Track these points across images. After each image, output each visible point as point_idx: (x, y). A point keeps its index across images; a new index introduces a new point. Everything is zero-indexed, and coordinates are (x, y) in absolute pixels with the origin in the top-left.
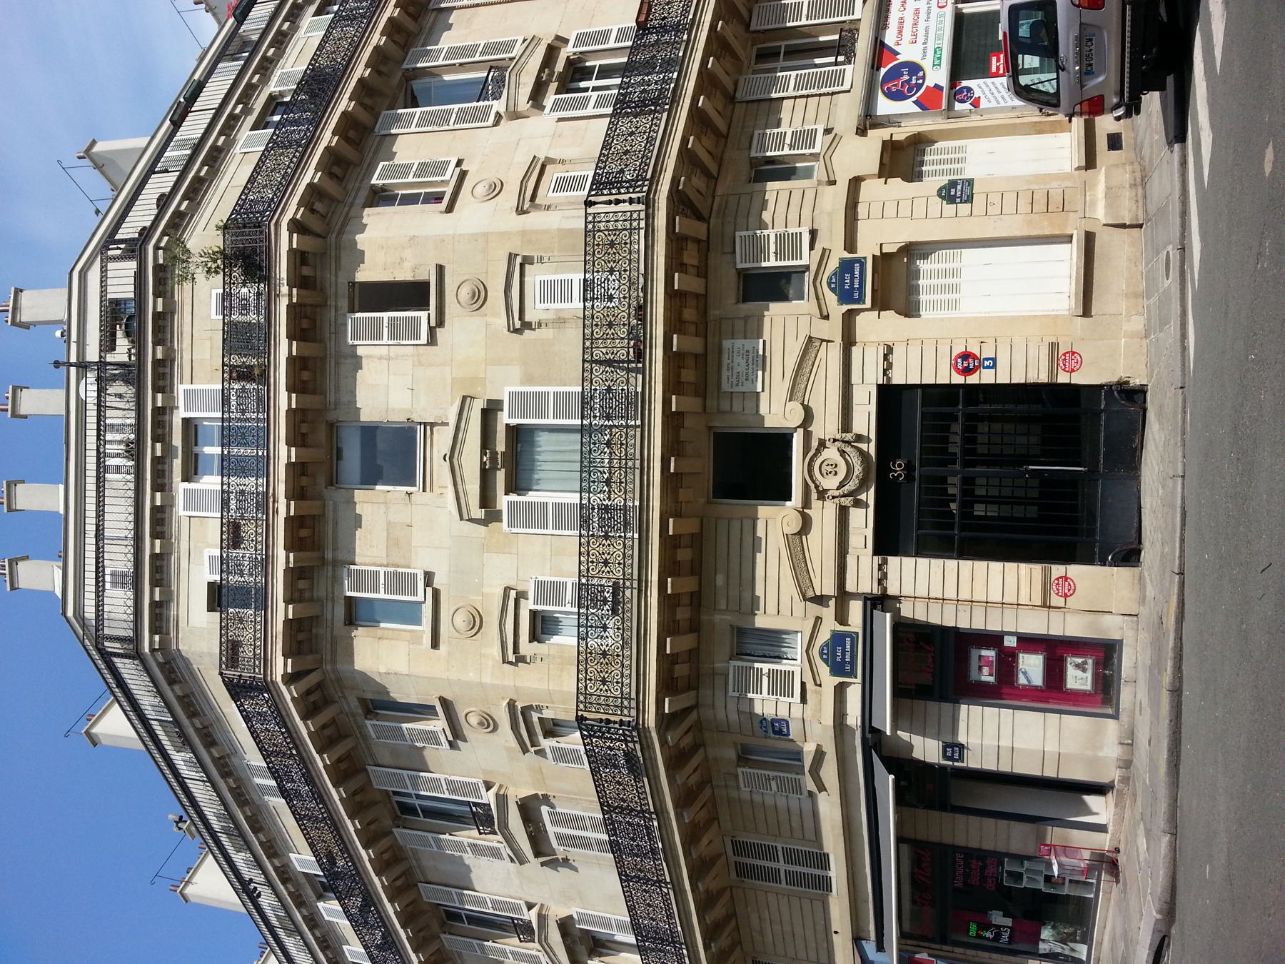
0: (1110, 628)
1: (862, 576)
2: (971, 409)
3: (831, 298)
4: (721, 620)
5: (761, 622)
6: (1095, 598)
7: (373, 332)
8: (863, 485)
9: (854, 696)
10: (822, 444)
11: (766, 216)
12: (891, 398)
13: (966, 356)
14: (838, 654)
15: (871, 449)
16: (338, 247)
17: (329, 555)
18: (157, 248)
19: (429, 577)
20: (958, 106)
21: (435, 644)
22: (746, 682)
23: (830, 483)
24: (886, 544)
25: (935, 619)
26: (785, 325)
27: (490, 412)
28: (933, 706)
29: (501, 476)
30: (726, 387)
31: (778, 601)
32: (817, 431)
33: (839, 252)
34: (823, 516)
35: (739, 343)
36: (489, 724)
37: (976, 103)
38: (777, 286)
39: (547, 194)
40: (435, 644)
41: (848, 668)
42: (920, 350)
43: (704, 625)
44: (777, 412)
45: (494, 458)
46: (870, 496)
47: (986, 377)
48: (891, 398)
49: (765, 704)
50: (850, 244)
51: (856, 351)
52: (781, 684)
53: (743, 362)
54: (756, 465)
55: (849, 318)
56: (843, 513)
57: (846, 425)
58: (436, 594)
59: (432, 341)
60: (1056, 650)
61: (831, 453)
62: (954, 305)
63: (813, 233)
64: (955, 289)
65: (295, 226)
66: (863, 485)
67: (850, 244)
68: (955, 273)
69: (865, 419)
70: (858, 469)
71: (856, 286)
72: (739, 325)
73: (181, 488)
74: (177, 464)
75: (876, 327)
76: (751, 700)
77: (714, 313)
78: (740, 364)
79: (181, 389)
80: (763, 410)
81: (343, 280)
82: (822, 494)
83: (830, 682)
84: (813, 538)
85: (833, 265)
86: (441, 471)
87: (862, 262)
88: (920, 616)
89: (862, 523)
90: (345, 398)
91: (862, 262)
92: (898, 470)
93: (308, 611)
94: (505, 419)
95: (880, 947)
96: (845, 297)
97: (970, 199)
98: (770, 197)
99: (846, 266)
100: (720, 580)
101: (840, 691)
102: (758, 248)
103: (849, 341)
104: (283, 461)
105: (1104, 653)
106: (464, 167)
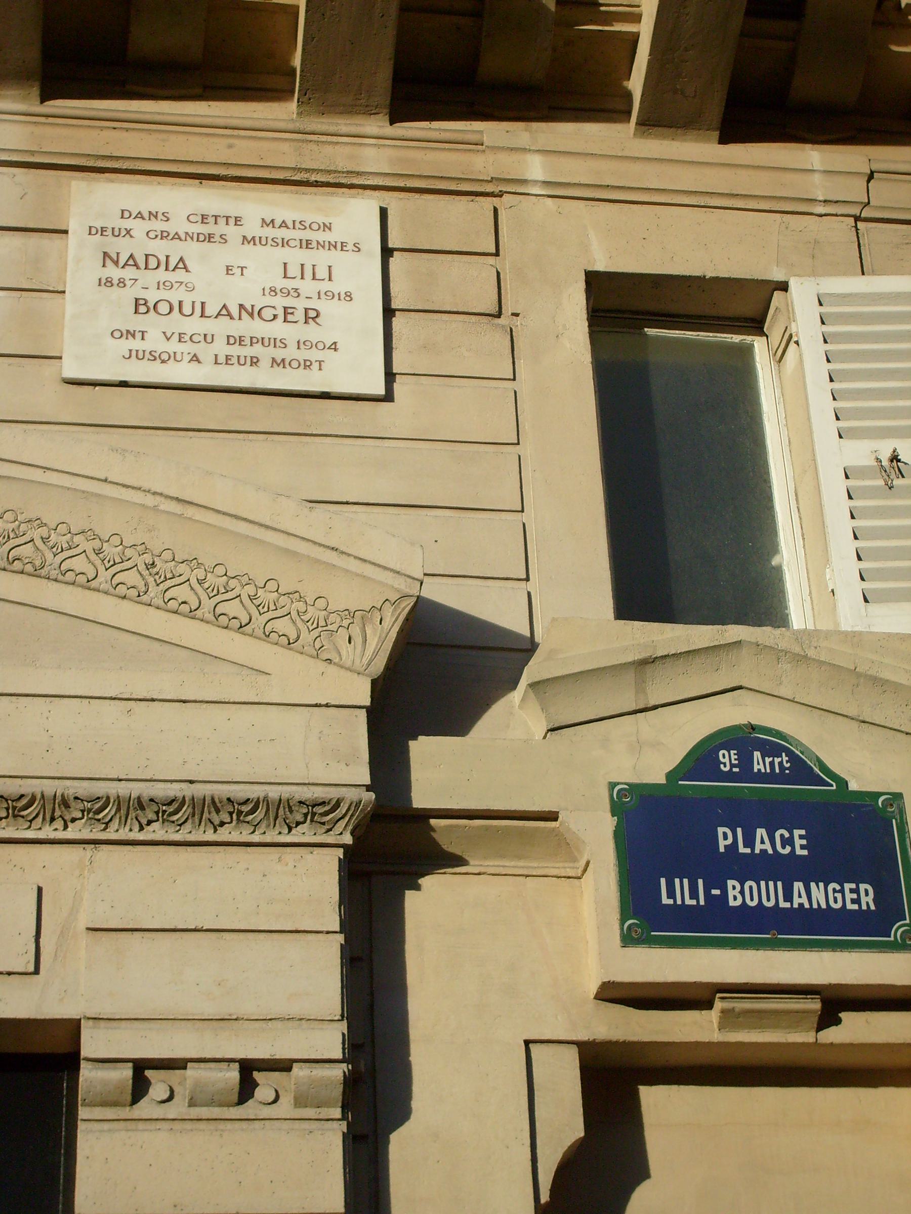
3: (654, 751)
30: (92, 203)
41: (680, 893)
53: (244, 289)
71: (737, 894)
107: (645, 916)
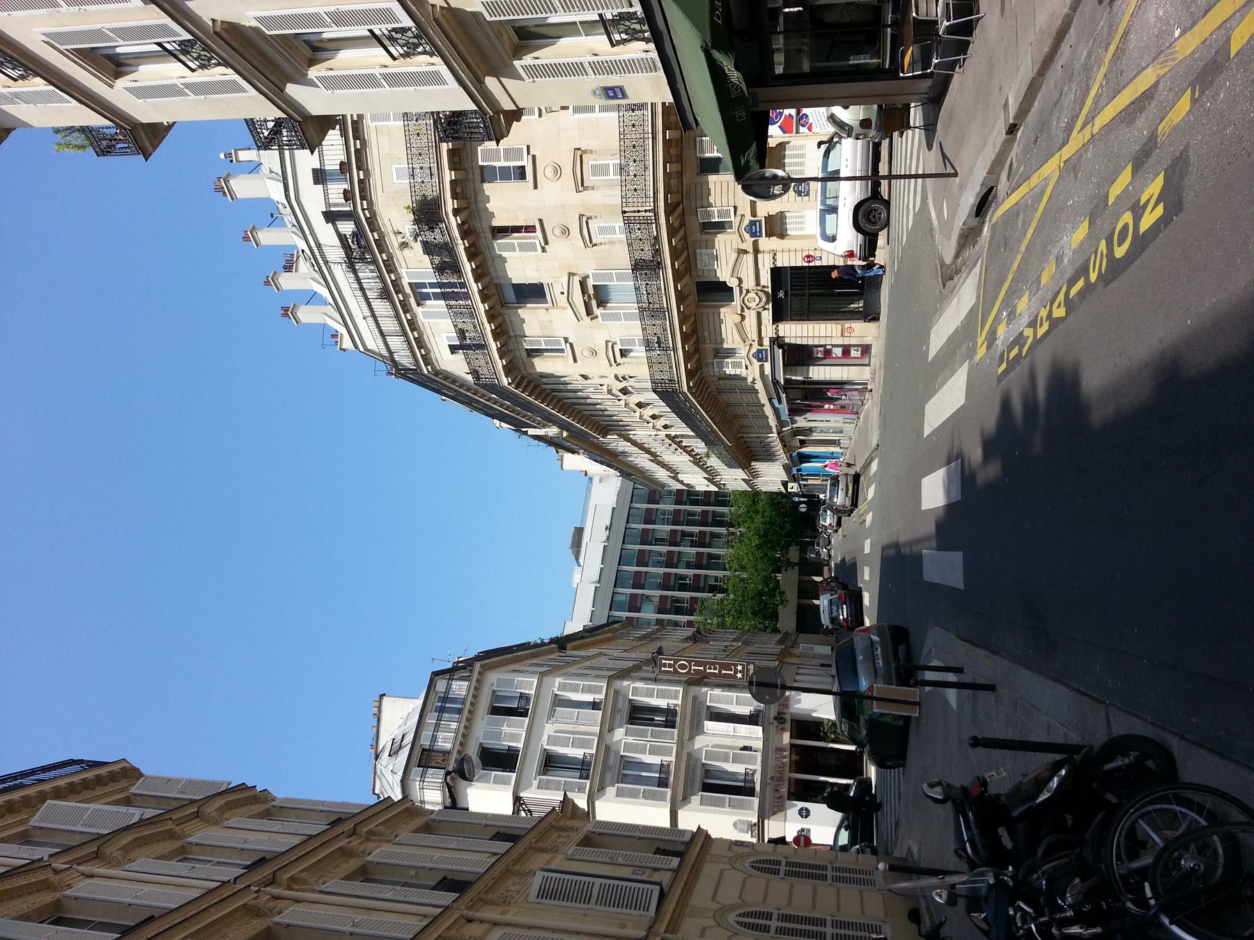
0: (867, 341)
1: (769, 331)
2: (822, 929)
4: (708, 347)
5: (725, 346)
6: (862, 331)
7: (511, 248)
8: (767, 303)
9: (767, 366)
10: (748, 291)
11: (711, 199)
12: (777, 273)
13: (808, 256)
14: (760, 356)
15: (770, 290)
16: (478, 211)
17: (512, 334)
18: (363, 210)
19: (566, 340)
20: (802, 129)
21: (575, 361)
22: (721, 366)
23: (753, 305)
24: (777, 319)
25: (799, 342)
26: (725, 244)
27: (583, 284)
28: (799, 368)
29: (594, 303)
31: (730, 337)
32: (745, 286)
33: (748, 218)
34: (751, 317)
35: (704, 251)
36: (594, 353)
37: (810, 129)
38: (721, 227)
39: (590, 179)
40: (575, 361)
42: (790, 254)
43: (701, 345)
44: (724, 274)
45: (589, 296)
46: (770, 306)
47: (818, 263)
48: (776, 272)
49: (730, 371)
50: (754, 214)
51: (760, 256)
52: (738, 365)
54: (719, 291)
55: (755, 244)
56: (759, 315)
57: (758, 284)
58: (571, 345)
59: (544, 250)
60: (846, 350)
61: (752, 295)
62: (802, 229)
63: (735, 208)
64: (802, 164)
65: (456, 212)
66: (767, 303)
67: (754, 214)
68: (802, 156)
69: (766, 279)
70: (764, 299)
72: (703, 243)
73: (419, 311)
74: (412, 300)
75: (765, 243)
76: (788, 698)
77: (690, 239)
78: (705, 259)
79: (403, 271)
80: (719, 275)
81: (485, 225)
82: (749, 308)
83: (757, 364)
84: (746, 322)
85: (746, 222)
86: (562, 300)
87: (760, 222)
88: (793, 341)
89: (767, 316)
90: (500, 274)
91: (760, 222)
92: (781, 294)
93: (510, 357)
94: (591, 282)
95: (780, 402)
96: (753, 235)
97: (808, 195)
98: (711, 186)
99: (752, 223)
100: (706, 334)
101: (762, 367)
102: (710, 215)
103: (756, 251)
104: (482, 310)
105: (866, 349)
106: (532, 153)
107: (761, 236)
